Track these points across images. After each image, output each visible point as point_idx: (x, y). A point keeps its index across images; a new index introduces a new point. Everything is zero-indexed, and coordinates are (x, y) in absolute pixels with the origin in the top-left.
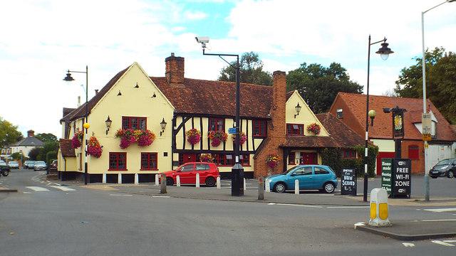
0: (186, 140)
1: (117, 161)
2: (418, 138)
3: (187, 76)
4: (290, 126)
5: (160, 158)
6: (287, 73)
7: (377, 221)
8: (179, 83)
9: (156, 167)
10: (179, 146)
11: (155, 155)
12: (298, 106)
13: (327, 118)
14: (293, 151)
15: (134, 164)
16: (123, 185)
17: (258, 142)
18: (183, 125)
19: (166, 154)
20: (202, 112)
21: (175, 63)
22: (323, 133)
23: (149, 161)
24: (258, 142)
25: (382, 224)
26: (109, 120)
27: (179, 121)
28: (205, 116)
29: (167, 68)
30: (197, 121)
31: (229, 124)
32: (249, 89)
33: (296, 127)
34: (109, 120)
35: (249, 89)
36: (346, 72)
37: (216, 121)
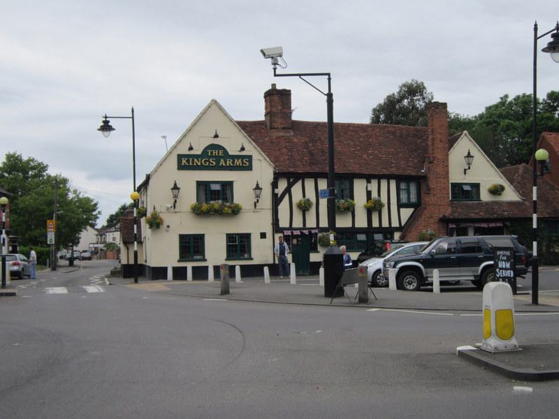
0: (386, 206)
1: (192, 246)
3: (296, 117)
4: (457, 187)
5: (255, 241)
7: (493, 343)
8: (283, 128)
9: (203, 253)
10: (284, 223)
11: (247, 237)
12: (469, 156)
13: (520, 172)
14: (463, 225)
15: (215, 253)
16: (222, 277)
17: (406, 213)
18: (288, 191)
19: (263, 235)
20: (316, 169)
21: (278, 99)
22: (510, 195)
23: (238, 245)
24: (406, 213)
25: (502, 348)
26: (176, 188)
27: (283, 185)
28: (389, 177)
29: (266, 108)
30: (310, 184)
31: (360, 187)
32: (393, 133)
33: (466, 188)
34: (176, 188)
35: (393, 133)
37: (340, 188)
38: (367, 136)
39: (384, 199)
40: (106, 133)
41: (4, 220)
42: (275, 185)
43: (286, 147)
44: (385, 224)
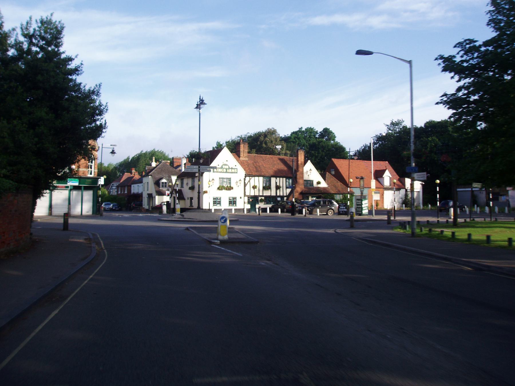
0: (282, 187)
2: (379, 189)
6: (336, 141)
7: (226, 237)
10: (248, 193)
17: (289, 190)
31: (273, 180)
36: (148, 151)
38: (273, 160)
39: (281, 185)
40: (113, 154)
41: (170, 189)
42: (245, 179)
43: (246, 165)
44: (281, 194)
